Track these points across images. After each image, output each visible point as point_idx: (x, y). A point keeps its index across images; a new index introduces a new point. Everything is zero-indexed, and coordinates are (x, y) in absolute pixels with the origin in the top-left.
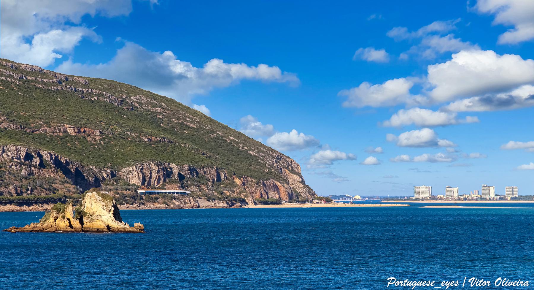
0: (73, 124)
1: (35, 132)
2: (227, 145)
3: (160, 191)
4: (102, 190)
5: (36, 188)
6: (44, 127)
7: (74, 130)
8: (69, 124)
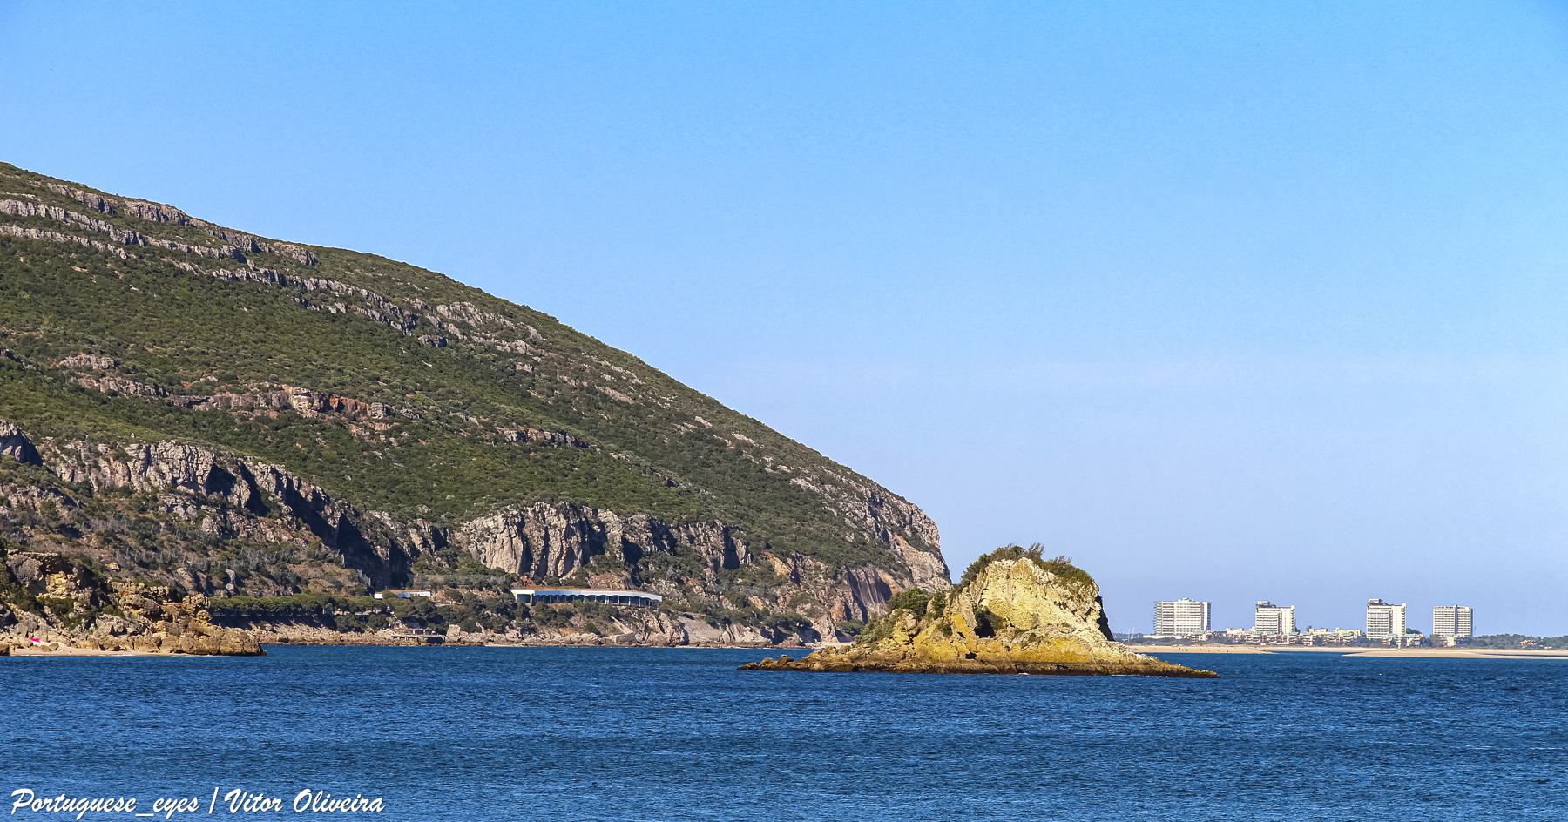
0: (306, 383)
1: (195, 407)
2: (727, 459)
3: (576, 592)
4: (411, 586)
5: (249, 576)
6: (221, 391)
7: (311, 402)
8: (296, 385)
